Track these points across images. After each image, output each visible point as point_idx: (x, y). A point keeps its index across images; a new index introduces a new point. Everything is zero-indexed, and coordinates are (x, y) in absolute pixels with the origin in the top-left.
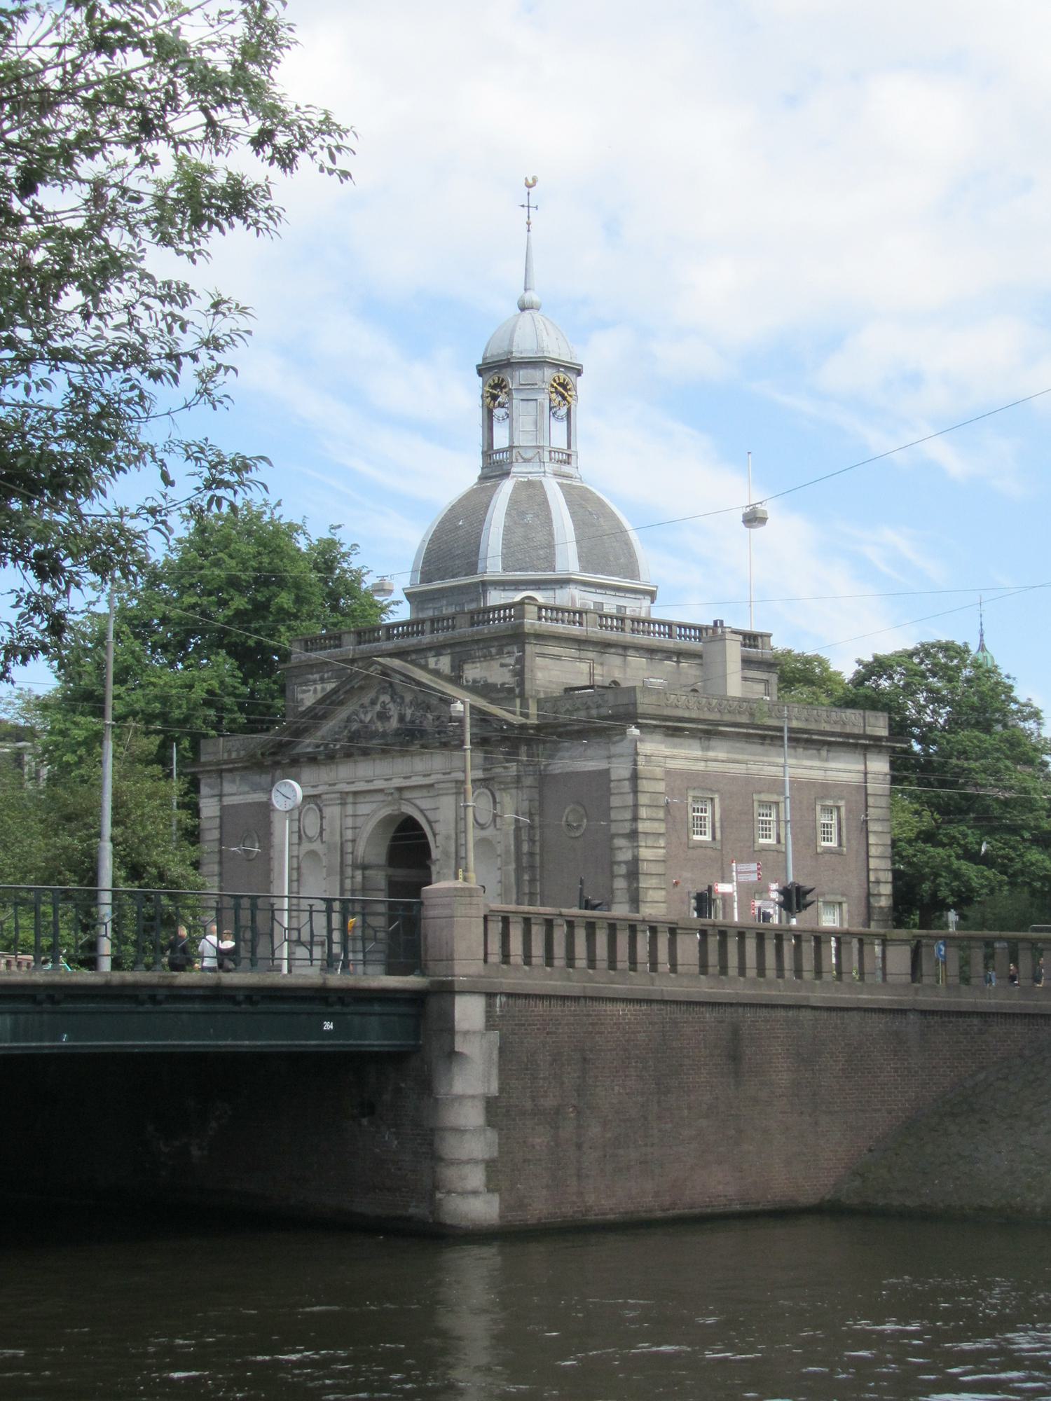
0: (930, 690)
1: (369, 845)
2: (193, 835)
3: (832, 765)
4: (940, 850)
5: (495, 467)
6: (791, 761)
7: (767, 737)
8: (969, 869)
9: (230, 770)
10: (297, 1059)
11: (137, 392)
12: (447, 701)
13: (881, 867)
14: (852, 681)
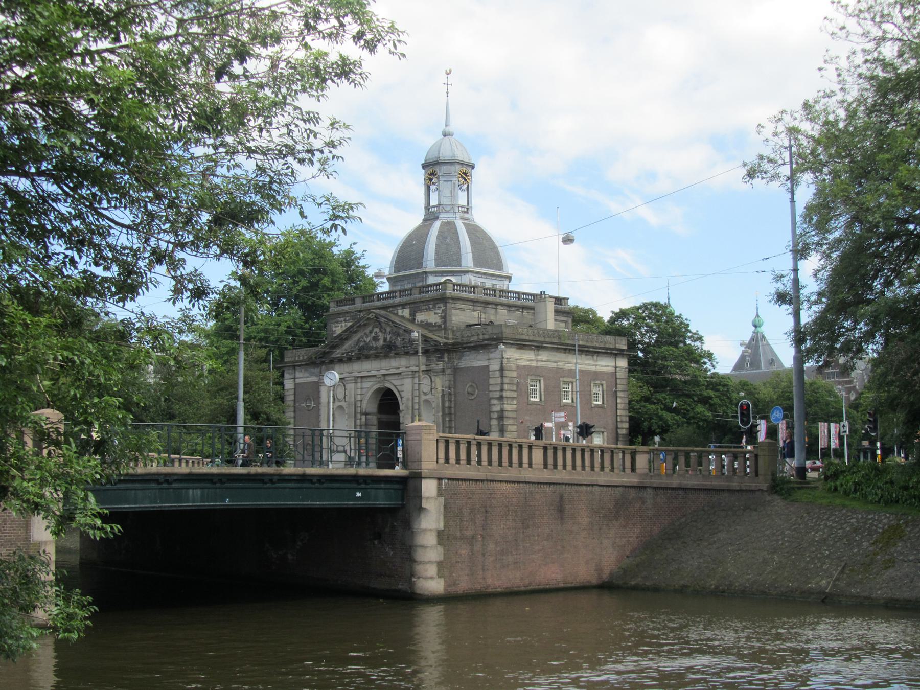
0: (647, 325)
1: (369, 404)
2: (282, 398)
3: (599, 363)
4: (653, 406)
5: (431, 216)
6: (579, 361)
7: (568, 349)
8: (667, 415)
9: (299, 366)
10: (340, 510)
11: (290, 170)
12: (409, 332)
13: (623, 414)
14: (609, 322)
